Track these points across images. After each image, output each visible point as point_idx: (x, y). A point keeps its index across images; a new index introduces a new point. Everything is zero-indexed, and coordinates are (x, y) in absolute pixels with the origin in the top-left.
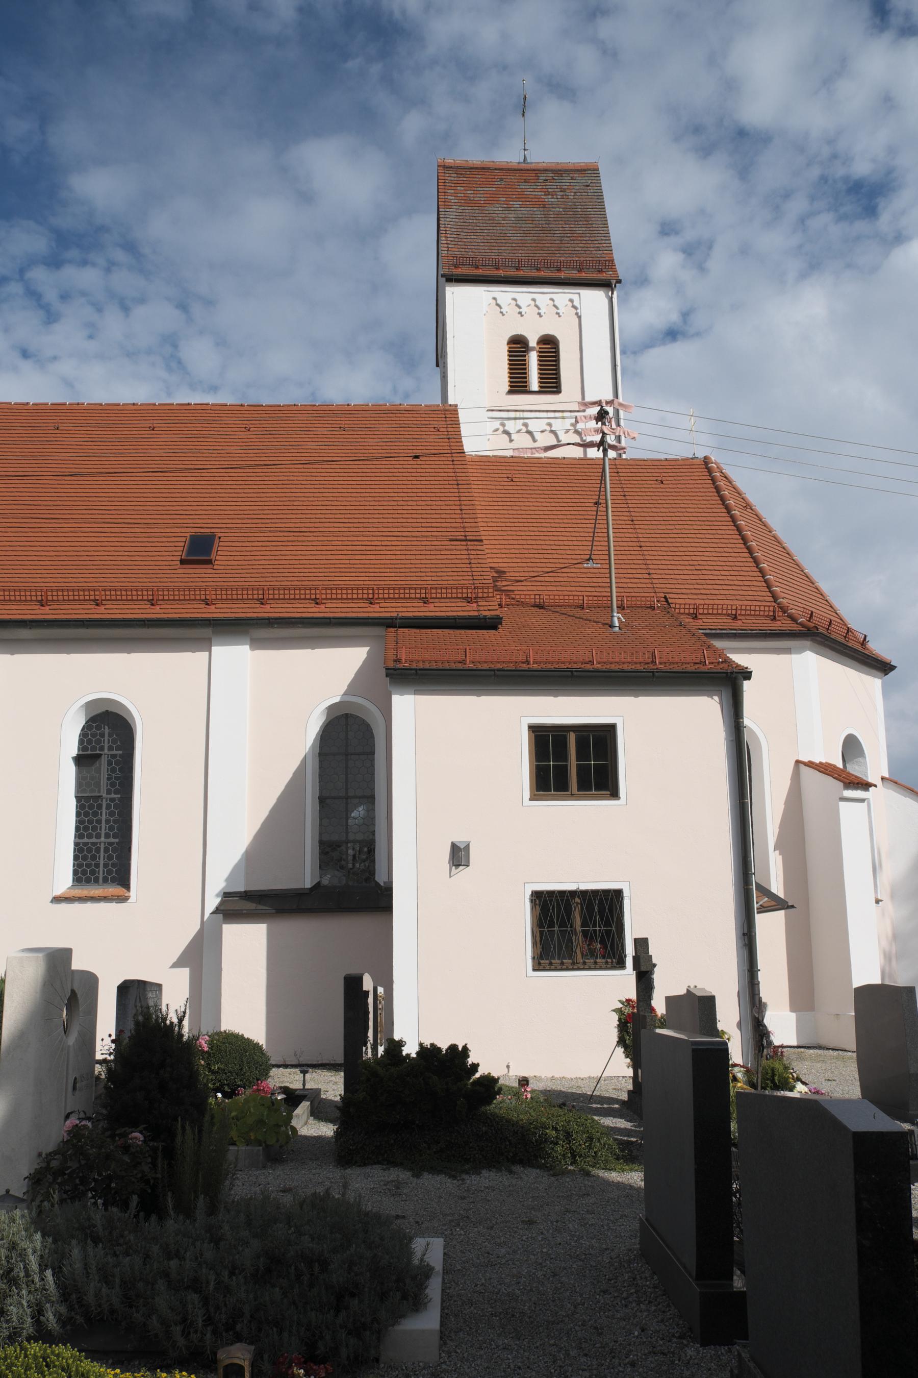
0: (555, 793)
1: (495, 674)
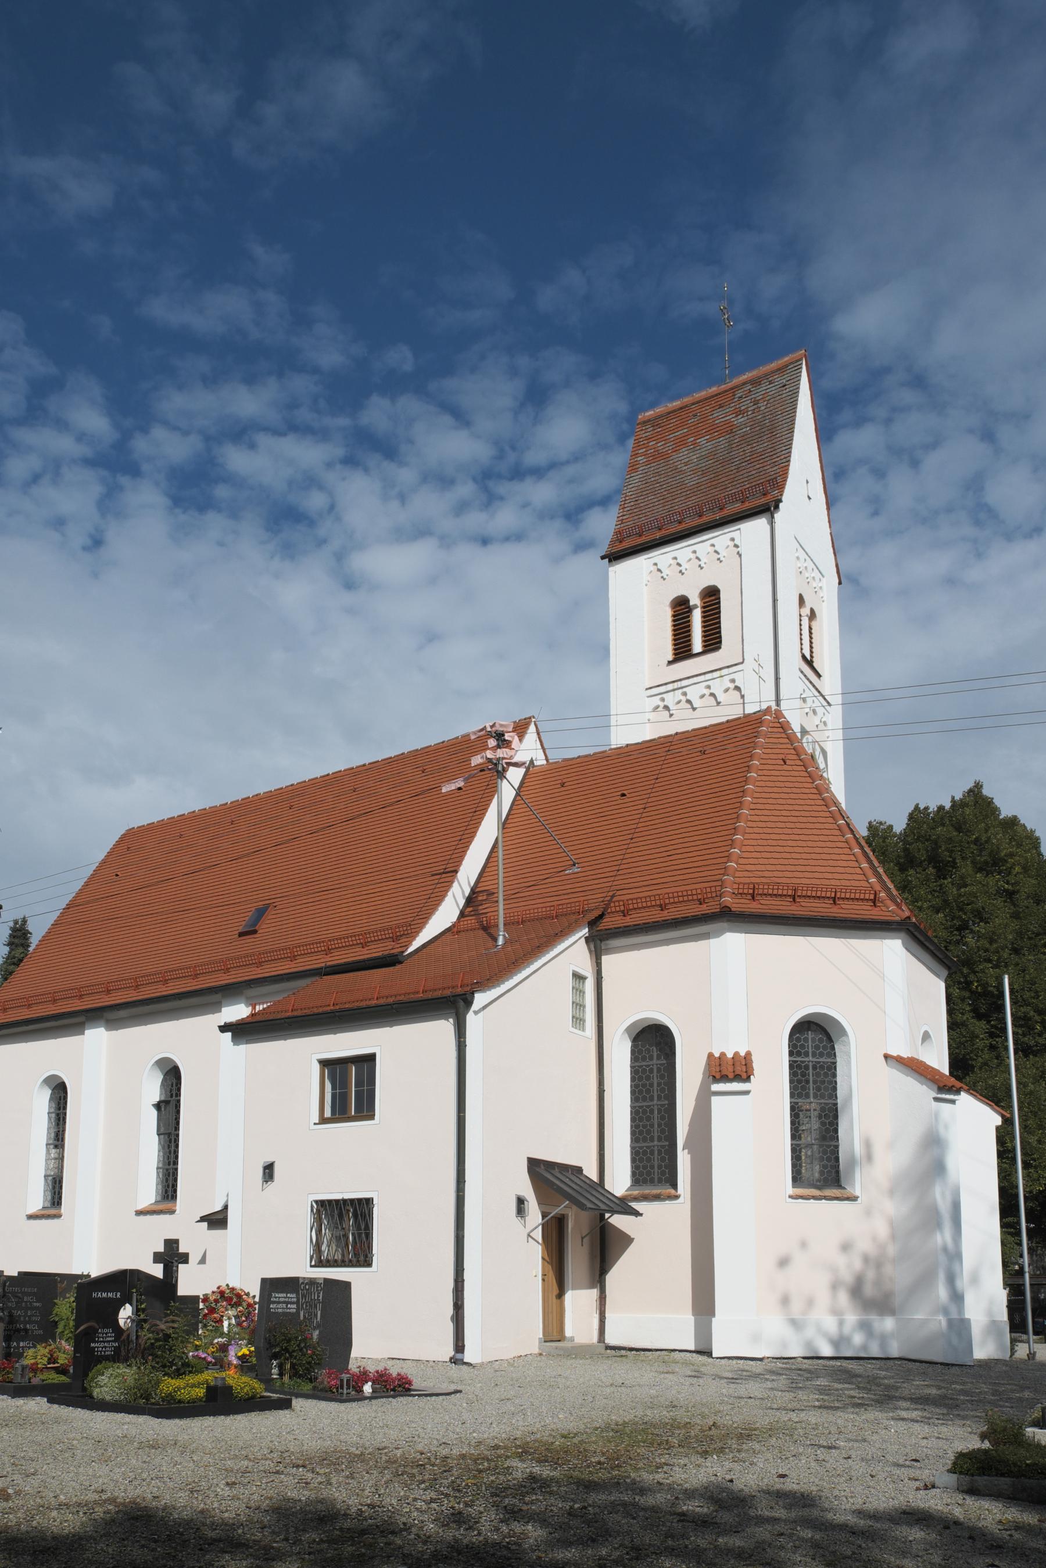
0: (340, 1116)
1: (392, 1008)
